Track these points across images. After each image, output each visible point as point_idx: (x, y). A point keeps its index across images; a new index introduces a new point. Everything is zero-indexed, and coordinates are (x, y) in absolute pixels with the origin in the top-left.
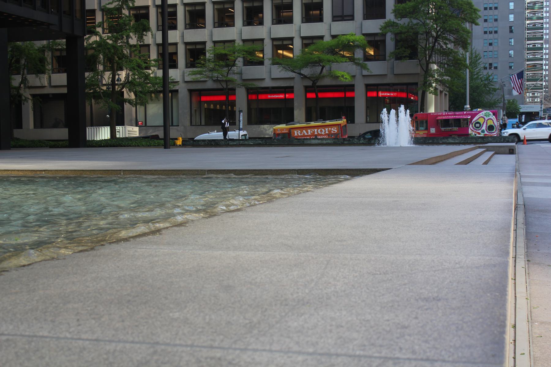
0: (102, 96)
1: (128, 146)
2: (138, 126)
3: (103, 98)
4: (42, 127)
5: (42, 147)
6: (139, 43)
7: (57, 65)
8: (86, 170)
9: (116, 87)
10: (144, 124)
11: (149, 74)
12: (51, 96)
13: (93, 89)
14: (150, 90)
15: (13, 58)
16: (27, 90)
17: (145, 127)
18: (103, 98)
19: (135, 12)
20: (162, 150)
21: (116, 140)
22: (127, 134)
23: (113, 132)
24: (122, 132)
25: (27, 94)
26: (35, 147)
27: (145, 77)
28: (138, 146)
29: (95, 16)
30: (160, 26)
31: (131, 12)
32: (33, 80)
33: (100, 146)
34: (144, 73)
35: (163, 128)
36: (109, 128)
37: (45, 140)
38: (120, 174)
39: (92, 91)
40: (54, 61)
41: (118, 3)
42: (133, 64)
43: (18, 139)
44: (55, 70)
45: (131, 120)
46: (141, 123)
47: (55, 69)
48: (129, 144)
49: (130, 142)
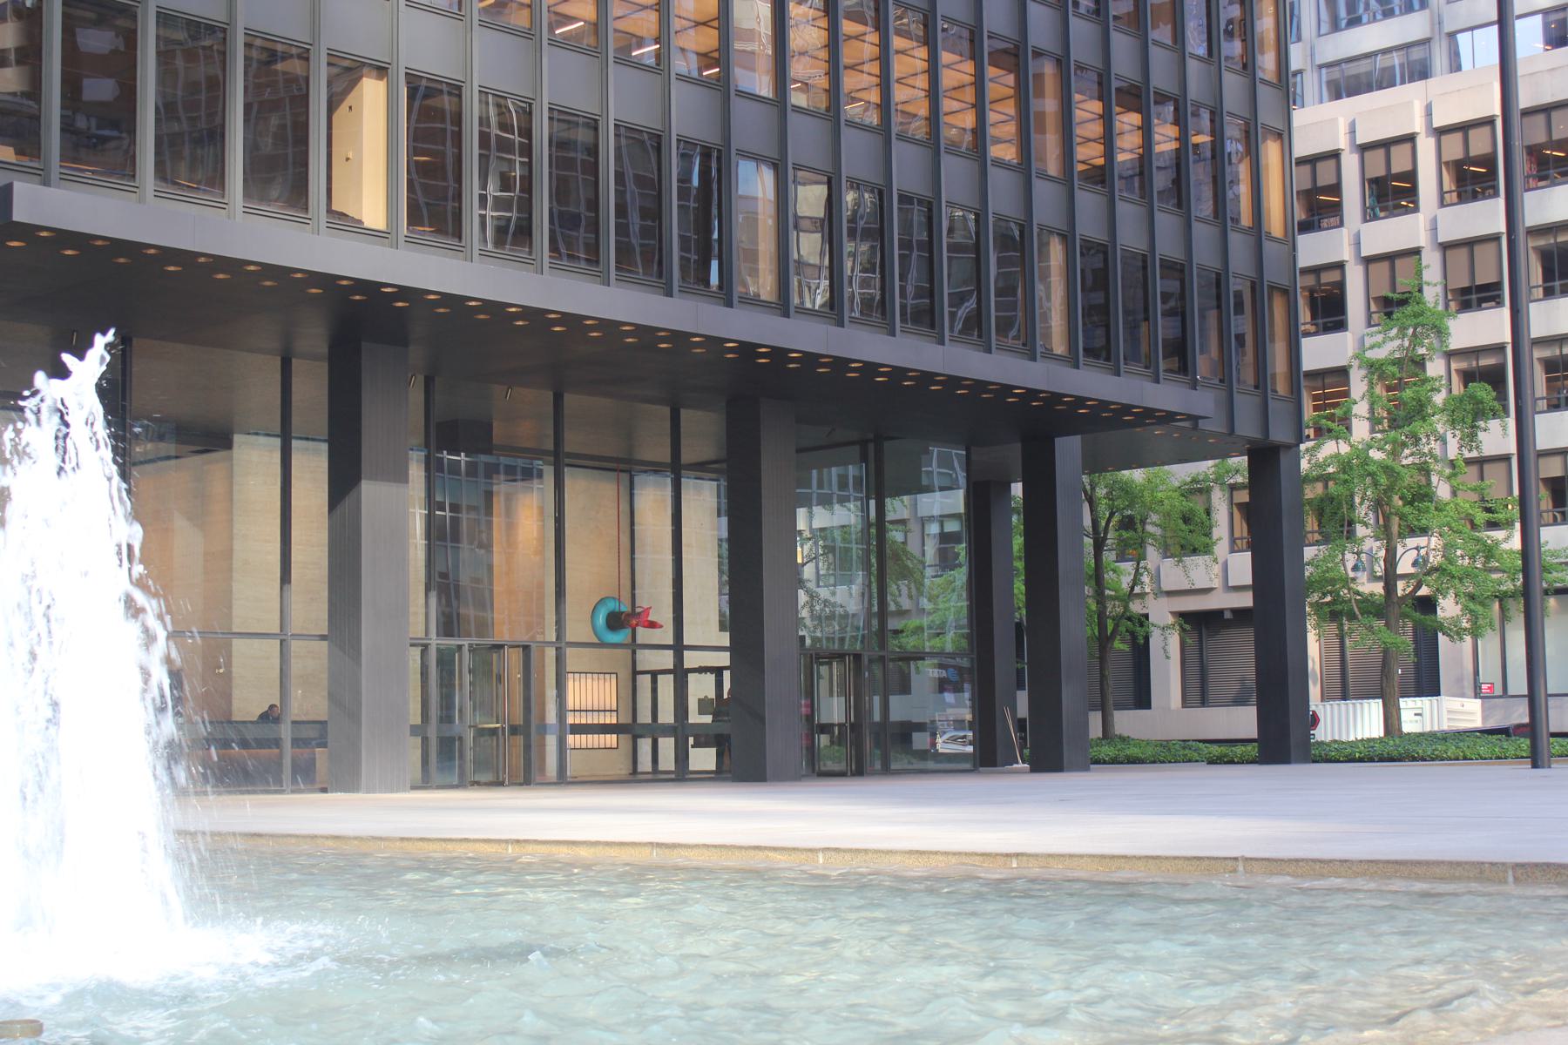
0: (1357, 613)
1: (1433, 760)
2: (1481, 698)
3: (1360, 617)
4: (1204, 702)
5: (1190, 761)
6: (1467, 455)
7: (1245, 526)
8: (1135, 857)
9: (1400, 585)
10: (1498, 691)
11: (1497, 543)
12: (1228, 615)
13: (1330, 593)
14: (1499, 591)
15: (1112, 515)
16: (1164, 600)
17: (1502, 700)
18: (1360, 617)
19: (1463, 365)
20: (1525, 769)
21: (1397, 741)
22: (1445, 720)
23: (1391, 719)
24: (1417, 715)
25: (1160, 613)
26: (1170, 762)
27: (1484, 551)
28: (1465, 758)
29: (1349, 386)
30: (1542, 398)
31: (1454, 366)
32: (1172, 574)
33: (1351, 759)
34: (1478, 540)
35: (1526, 701)
36: (714, 769)
37: (1200, 741)
38: (1235, 871)
39: (1328, 599)
40: (1237, 515)
41: (1399, 342)
42: (1446, 516)
43: (1123, 739)
44: (1239, 542)
45: (1460, 680)
46: (1489, 688)
47: (1238, 539)
48: (1436, 753)
49: (1439, 747)
